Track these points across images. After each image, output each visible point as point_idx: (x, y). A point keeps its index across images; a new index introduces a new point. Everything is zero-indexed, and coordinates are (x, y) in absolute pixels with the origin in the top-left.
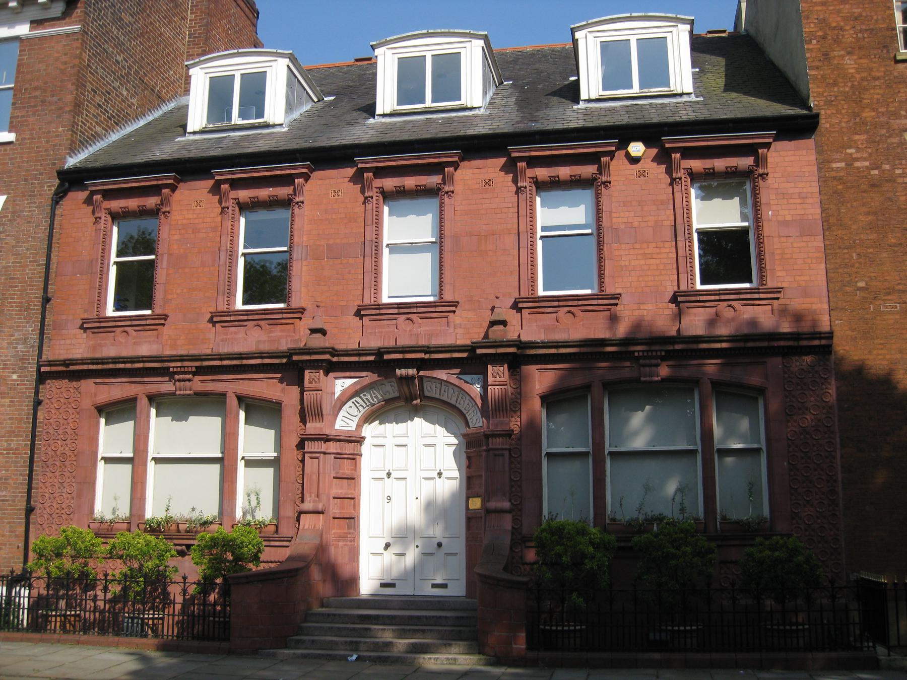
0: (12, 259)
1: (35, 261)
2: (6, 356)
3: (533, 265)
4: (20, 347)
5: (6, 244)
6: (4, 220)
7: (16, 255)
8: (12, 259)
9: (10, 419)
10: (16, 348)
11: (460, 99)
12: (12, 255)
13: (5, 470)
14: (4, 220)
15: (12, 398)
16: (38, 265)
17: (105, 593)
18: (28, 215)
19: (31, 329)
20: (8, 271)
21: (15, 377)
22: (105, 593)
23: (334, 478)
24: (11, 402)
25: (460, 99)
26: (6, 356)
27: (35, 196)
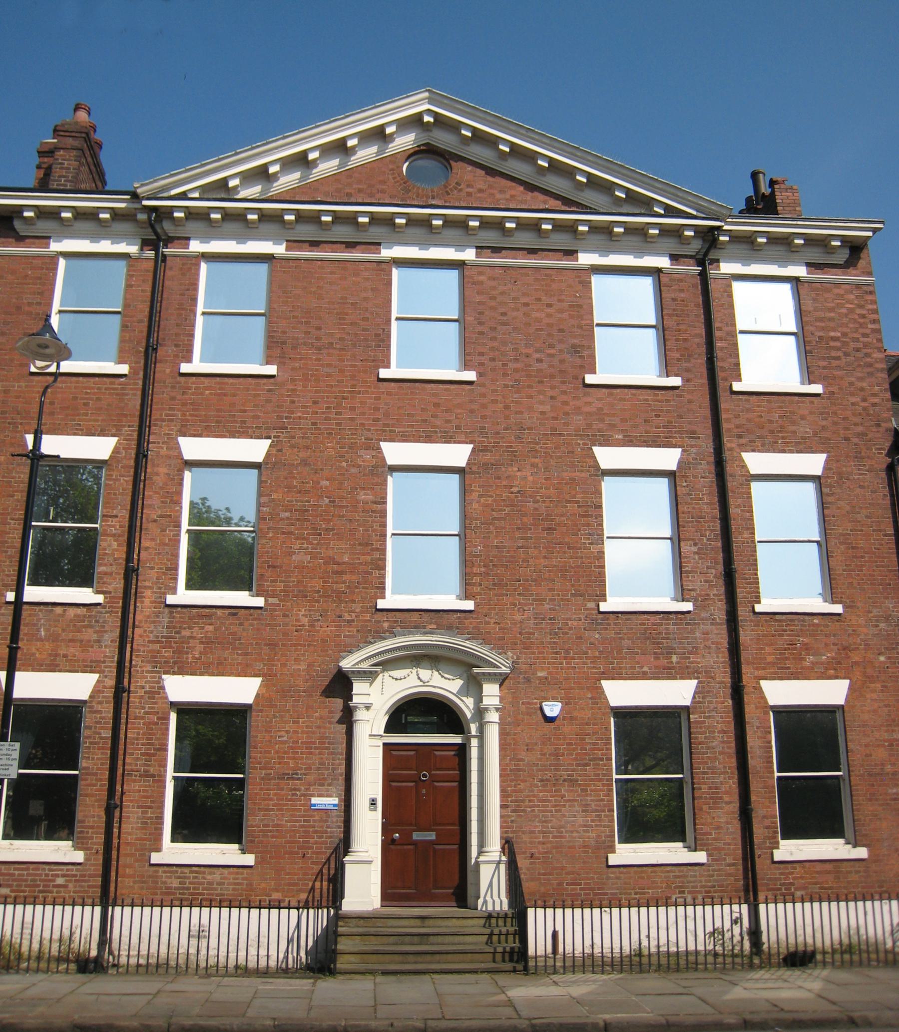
0: (850, 526)
1: (880, 531)
2: (865, 635)
3: (42, 233)
4: (882, 625)
5: (839, 508)
6: (829, 481)
7: (853, 521)
8: (850, 526)
9: (886, 706)
10: (877, 626)
11: (619, 843)
12: (850, 522)
13: (891, 764)
14: (829, 481)
15: (884, 682)
16: (886, 535)
17: (39, 963)
18: (858, 479)
19: (891, 605)
20: (848, 539)
21: (882, 658)
22: (39, 963)
23: (766, 897)
24: (883, 686)
25: (619, 843)
26: (865, 635)
27: (863, 458)
